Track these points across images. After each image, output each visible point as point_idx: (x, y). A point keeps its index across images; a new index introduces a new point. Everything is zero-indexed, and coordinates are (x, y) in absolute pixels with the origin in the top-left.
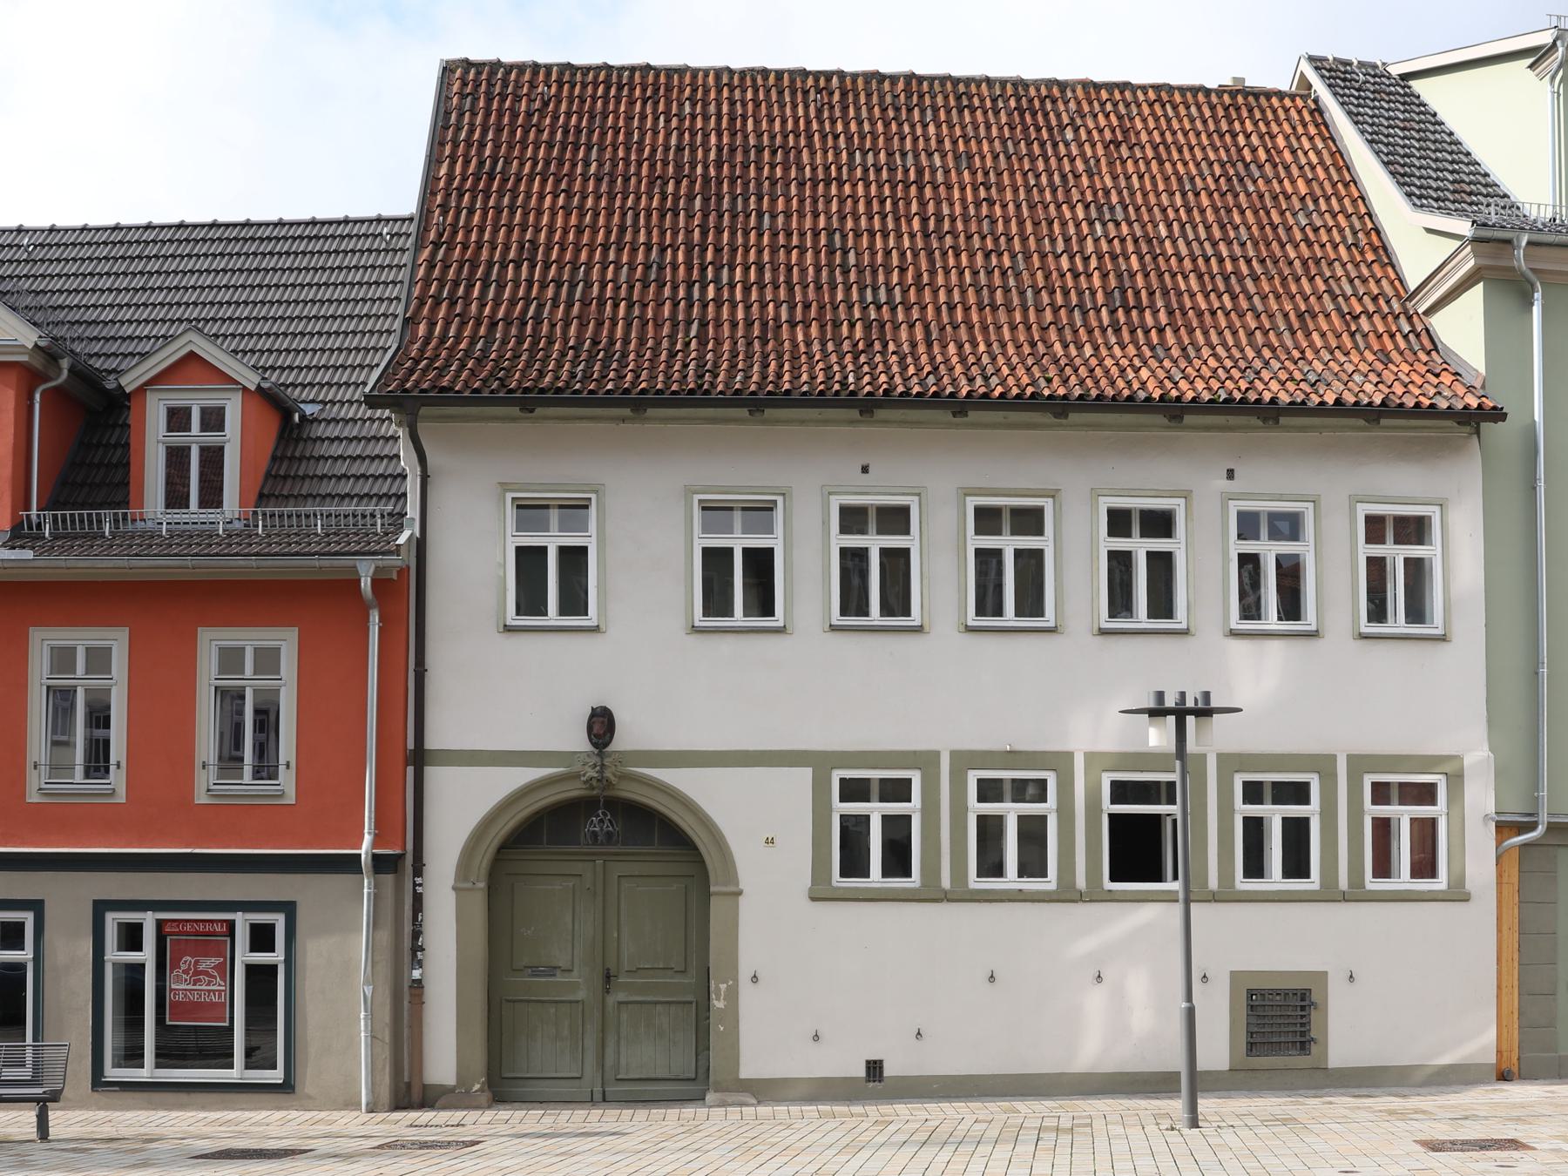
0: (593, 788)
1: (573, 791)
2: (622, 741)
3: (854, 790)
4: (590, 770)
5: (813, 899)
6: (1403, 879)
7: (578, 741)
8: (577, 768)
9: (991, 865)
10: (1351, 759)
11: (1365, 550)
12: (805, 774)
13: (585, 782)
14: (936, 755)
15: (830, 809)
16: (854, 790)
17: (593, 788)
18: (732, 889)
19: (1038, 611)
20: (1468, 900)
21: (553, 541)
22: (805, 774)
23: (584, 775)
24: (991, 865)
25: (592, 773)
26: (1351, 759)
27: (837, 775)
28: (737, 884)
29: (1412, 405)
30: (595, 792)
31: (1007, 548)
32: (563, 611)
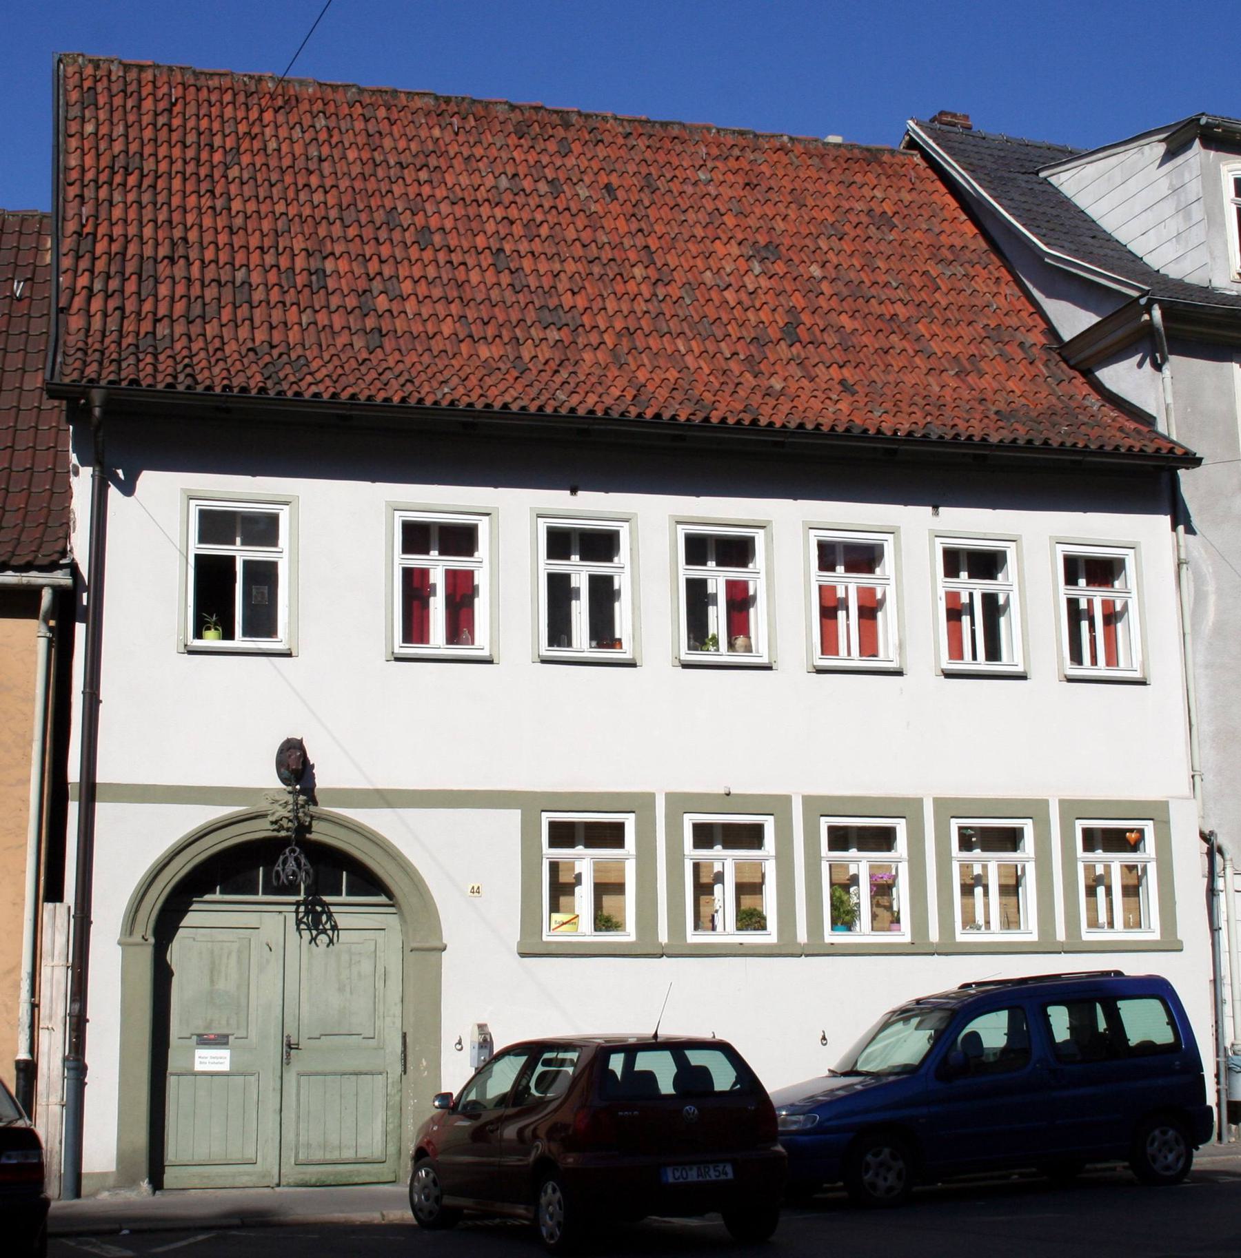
0: (281, 828)
1: (260, 830)
2: (323, 779)
3: (563, 835)
4: (280, 808)
5: (523, 955)
6: (727, 931)
7: (269, 779)
8: (263, 805)
9: (844, 917)
10: (670, 797)
11: (686, 572)
12: (513, 817)
13: (272, 823)
14: (651, 797)
15: (950, 858)
16: (563, 835)
17: (281, 828)
18: (434, 943)
19: (1096, 664)
20: (1181, 950)
21: (242, 553)
22: (513, 817)
23: (273, 814)
24: (844, 917)
25: (283, 812)
26: (670, 797)
27: (546, 818)
28: (441, 938)
29: (765, 423)
30: (283, 834)
31: (579, 573)
32: (249, 631)
